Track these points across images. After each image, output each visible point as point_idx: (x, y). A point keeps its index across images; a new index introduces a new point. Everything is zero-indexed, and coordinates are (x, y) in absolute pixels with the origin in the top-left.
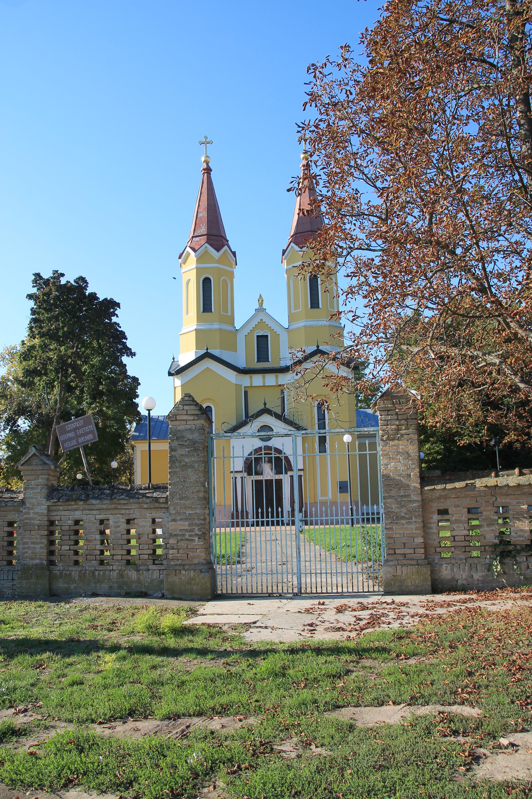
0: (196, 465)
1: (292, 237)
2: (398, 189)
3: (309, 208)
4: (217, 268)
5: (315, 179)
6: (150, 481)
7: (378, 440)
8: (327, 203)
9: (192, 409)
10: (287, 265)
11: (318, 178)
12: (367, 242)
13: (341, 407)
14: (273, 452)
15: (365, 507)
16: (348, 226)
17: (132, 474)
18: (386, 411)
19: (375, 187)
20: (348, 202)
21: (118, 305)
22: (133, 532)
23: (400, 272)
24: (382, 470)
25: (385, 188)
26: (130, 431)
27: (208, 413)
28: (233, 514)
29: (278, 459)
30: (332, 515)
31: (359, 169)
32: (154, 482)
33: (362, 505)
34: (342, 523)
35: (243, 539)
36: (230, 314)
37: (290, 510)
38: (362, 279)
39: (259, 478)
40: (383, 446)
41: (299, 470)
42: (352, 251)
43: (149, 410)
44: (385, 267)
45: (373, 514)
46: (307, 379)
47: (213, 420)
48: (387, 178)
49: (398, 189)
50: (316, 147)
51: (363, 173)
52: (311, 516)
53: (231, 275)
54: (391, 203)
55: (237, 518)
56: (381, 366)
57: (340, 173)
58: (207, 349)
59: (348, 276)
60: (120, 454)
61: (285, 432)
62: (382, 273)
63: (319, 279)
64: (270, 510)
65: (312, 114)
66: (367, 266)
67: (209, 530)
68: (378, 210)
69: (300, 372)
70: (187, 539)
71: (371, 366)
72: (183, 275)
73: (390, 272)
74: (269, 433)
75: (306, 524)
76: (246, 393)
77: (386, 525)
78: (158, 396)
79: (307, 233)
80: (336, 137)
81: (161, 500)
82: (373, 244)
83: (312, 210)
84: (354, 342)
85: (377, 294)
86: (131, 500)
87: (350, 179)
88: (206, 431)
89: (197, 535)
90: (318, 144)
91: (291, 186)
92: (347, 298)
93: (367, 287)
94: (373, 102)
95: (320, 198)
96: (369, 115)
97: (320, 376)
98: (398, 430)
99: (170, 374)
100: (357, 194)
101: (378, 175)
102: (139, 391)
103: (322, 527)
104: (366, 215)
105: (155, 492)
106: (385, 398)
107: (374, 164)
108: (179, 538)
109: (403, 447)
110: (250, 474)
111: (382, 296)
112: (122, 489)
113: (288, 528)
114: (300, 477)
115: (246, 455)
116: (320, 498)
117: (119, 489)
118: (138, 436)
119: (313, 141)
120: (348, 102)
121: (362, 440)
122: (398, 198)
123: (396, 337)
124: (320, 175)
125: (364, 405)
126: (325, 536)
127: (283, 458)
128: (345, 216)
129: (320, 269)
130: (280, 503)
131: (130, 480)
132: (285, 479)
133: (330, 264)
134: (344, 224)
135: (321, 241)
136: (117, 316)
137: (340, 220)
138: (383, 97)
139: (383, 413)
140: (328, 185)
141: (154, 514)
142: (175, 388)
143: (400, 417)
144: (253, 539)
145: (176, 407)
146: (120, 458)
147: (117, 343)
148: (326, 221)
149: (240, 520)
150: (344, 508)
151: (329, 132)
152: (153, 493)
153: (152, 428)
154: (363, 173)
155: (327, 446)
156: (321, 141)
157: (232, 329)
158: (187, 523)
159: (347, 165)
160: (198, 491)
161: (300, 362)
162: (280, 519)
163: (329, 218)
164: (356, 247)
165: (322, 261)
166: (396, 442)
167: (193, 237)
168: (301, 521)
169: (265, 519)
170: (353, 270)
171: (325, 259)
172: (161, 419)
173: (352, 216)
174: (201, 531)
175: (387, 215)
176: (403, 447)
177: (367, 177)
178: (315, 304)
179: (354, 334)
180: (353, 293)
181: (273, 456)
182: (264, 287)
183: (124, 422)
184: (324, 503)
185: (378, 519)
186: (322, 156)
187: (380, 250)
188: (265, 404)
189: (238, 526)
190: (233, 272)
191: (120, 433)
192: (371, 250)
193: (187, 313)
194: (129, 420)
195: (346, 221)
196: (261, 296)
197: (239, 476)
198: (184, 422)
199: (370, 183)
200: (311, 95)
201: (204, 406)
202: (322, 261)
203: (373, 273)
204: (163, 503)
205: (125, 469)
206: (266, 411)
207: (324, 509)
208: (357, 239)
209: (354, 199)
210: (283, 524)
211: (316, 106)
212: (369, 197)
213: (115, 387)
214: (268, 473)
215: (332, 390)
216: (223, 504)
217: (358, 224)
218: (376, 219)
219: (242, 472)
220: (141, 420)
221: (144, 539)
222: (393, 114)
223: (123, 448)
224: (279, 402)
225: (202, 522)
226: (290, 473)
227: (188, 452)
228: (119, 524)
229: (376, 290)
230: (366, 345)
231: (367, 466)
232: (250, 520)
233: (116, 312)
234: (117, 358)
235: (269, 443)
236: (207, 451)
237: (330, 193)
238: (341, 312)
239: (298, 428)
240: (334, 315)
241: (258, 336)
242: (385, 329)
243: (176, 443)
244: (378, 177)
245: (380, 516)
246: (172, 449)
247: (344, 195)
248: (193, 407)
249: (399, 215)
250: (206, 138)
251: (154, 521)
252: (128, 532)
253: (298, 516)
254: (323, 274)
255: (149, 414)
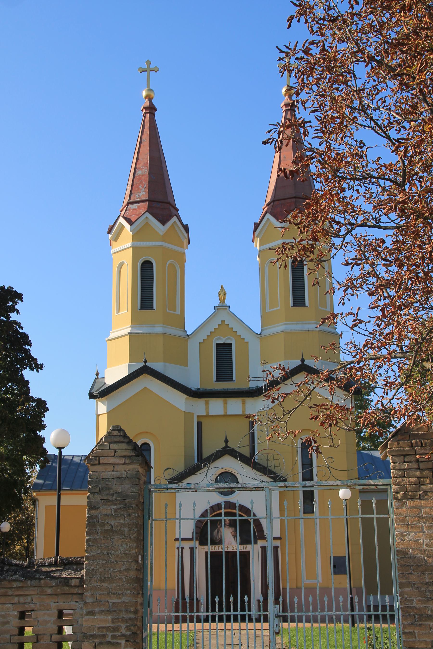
0: (126, 530)
1: (268, 205)
2: (421, 141)
3: (292, 167)
4: (162, 247)
5: (303, 127)
6: (57, 554)
7: (390, 497)
8: (319, 162)
9: (122, 449)
10: (260, 245)
11: (306, 125)
12: (375, 215)
13: (336, 451)
14: (237, 512)
15: (372, 598)
16: (348, 193)
17: (30, 540)
18: (402, 456)
19: (388, 137)
20: (349, 160)
21: (20, 296)
22: (28, 630)
23: (423, 258)
24: (395, 543)
25: (402, 139)
26: (30, 477)
27: (145, 453)
28: (177, 603)
29: (245, 524)
30: (323, 610)
31: (365, 113)
32: (64, 554)
33: (368, 593)
34: (338, 620)
35: (191, 642)
36: (178, 312)
37: (261, 599)
38: (368, 268)
39: (217, 549)
40: (398, 508)
41: (275, 538)
42: (353, 229)
43: (60, 448)
44: (400, 251)
45: (384, 608)
46: (287, 409)
47: (152, 464)
48: (406, 124)
49: (421, 141)
50: (305, 81)
51: (371, 119)
52: (292, 610)
53: (181, 258)
54: (411, 161)
55: (184, 610)
56: (394, 391)
57: (337, 118)
58: (145, 362)
59: (347, 264)
60: (14, 510)
61: (255, 483)
62: (397, 259)
63: (306, 268)
64: (231, 599)
65: (301, 34)
66: (375, 250)
67: (143, 628)
68: (391, 171)
69: (277, 399)
70: (109, 643)
71: (379, 391)
72: (114, 256)
73: (408, 259)
74: (232, 485)
75: (285, 621)
76: (199, 424)
77: (404, 626)
78: (73, 428)
79: (289, 201)
80: (333, 68)
81: (73, 582)
82: (384, 219)
83: (298, 170)
84: (355, 357)
85: (388, 290)
86: (29, 583)
87: (353, 126)
88: (142, 481)
89: (123, 635)
90: (308, 76)
91: (268, 136)
92: (345, 294)
93: (375, 280)
94: (387, 15)
95: (308, 153)
96: (381, 34)
97: (306, 405)
98: (419, 484)
99: (92, 396)
100: (361, 147)
101: (392, 121)
102: (47, 419)
103: (308, 625)
104: (374, 178)
105: (65, 569)
106: (399, 437)
107: (387, 104)
108: (97, 641)
109: (428, 510)
110: (203, 542)
111: (397, 292)
112: (16, 565)
113: (258, 625)
114: (276, 548)
115: (197, 516)
116: (305, 581)
117: (12, 565)
118: (42, 485)
119: (300, 73)
120: (352, 15)
121: (367, 497)
122: (421, 153)
123: (416, 351)
124: (309, 122)
125: (368, 445)
126: (313, 641)
127: (252, 522)
128: (344, 179)
129: (308, 253)
130: (246, 590)
131: (27, 549)
132: (254, 551)
133: (322, 245)
134: (343, 190)
135: (309, 213)
136: (18, 312)
137: (337, 185)
138: (403, 9)
139: (397, 459)
140: (321, 135)
141: (62, 603)
142: (98, 416)
143: (422, 466)
144: (206, 643)
145: (99, 445)
146: (15, 517)
147: (16, 351)
148: (318, 186)
149: (188, 614)
150: (341, 599)
151: (324, 60)
152: (61, 571)
153: (64, 473)
154: (371, 119)
155: (316, 505)
156: (312, 73)
157: (179, 333)
158: (110, 618)
159: (348, 107)
160: (127, 570)
161: (274, 384)
162: (246, 613)
163: (321, 182)
164: (359, 222)
165: (310, 242)
166: (417, 502)
167: (128, 204)
168: (277, 616)
169: (224, 613)
170: (354, 255)
171: (315, 239)
172: (76, 460)
173: (354, 179)
174: (130, 630)
175: (404, 178)
176: (428, 510)
177: (377, 124)
178: (299, 300)
179: (355, 346)
180: (353, 287)
181: (237, 518)
182: (227, 274)
183: (22, 464)
184: (311, 590)
185: (392, 617)
186: (313, 95)
187: (393, 228)
188: (226, 441)
189: (184, 621)
190: (183, 254)
191: (15, 481)
192: (380, 227)
193: (118, 311)
194: (30, 462)
195: (345, 186)
196: (222, 288)
197: (187, 545)
198: (111, 468)
199: (380, 132)
200: (300, 5)
201: (139, 443)
202: (310, 242)
203: (383, 259)
204: (75, 586)
205: (21, 533)
206: (227, 451)
207: (311, 599)
208: (361, 212)
209: (357, 154)
210: (251, 620)
211: (306, 22)
212: (380, 152)
213: (12, 413)
214: (230, 542)
215: (323, 424)
216: (163, 586)
217: (362, 190)
218: (388, 183)
219: (191, 539)
220: (48, 462)
221: (45, 641)
222: (416, 32)
223: (19, 502)
224: (247, 441)
225: (132, 616)
226: (261, 543)
227: (116, 511)
228: (8, 619)
229: (387, 285)
230: (372, 361)
231: (374, 536)
232: (203, 614)
233: (17, 307)
234: (16, 371)
235: (232, 498)
236: (143, 510)
237: (324, 146)
238: (337, 315)
239: (276, 477)
240: (327, 319)
241: (218, 345)
242: (399, 339)
243: (98, 497)
244: (392, 124)
245: (395, 613)
246: (92, 506)
247: (343, 149)
248: (124, 446)
249: (421, 177)
250: (149, 63)
251: (60, 614)
252: (21, 631)
253: (273, 609)
254: (312, 260)
255: (60, 453)
